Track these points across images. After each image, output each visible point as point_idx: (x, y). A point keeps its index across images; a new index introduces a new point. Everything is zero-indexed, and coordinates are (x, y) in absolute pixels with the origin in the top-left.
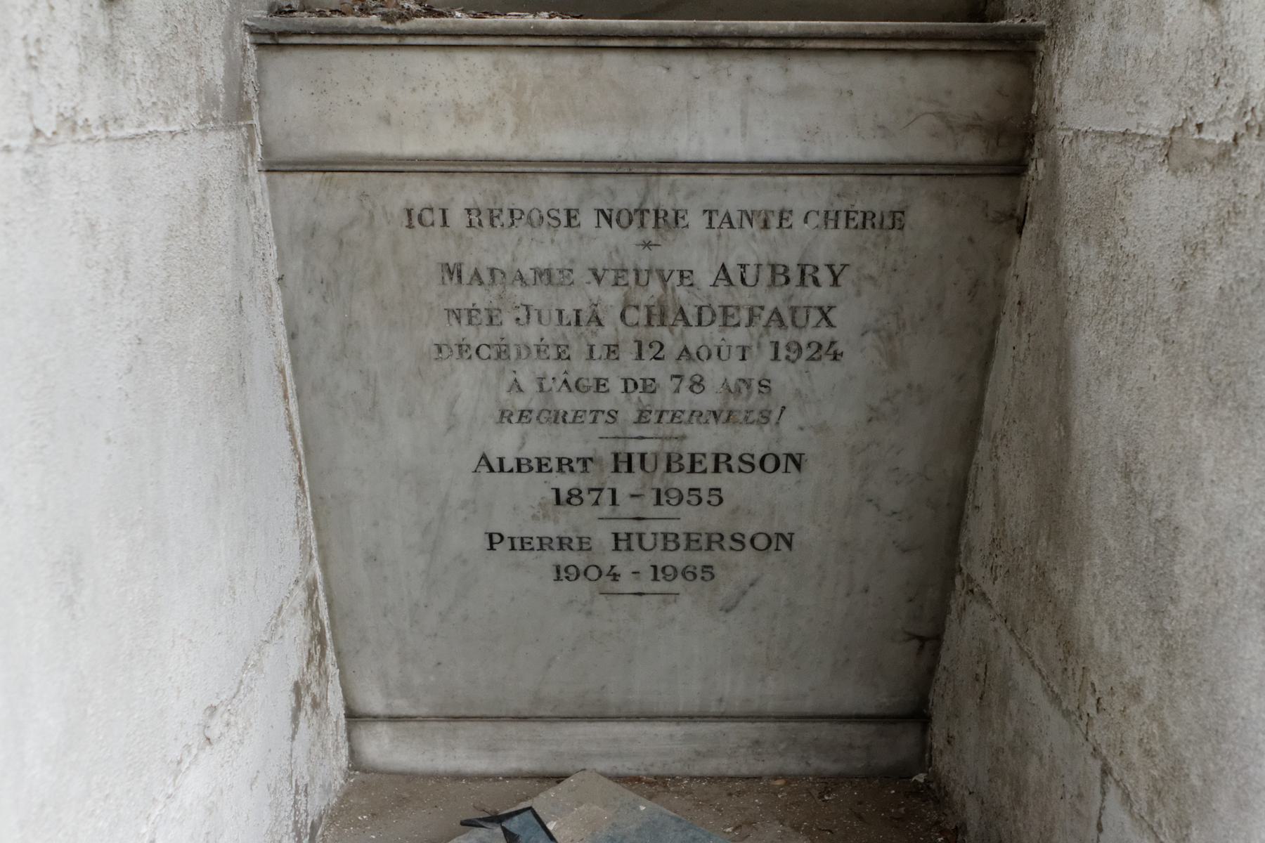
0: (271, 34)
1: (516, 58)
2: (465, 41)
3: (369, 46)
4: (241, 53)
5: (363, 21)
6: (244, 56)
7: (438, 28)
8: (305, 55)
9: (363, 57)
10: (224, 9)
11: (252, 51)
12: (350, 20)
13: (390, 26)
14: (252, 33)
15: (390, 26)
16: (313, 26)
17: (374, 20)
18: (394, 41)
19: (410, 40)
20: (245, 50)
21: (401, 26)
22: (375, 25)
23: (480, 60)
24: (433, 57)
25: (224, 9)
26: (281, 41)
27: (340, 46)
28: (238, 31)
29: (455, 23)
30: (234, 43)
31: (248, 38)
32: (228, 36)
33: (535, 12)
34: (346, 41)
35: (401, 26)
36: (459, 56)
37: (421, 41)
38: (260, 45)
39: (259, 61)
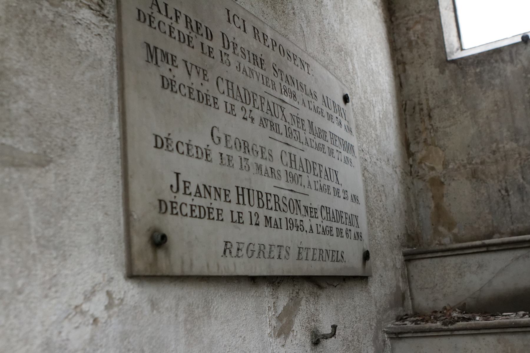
0: (395, 334)
1: (508, 337)
2: (481, 332)
3: (431, 336)
4: (382, 344)
5: (433, 325)
6: (384, 345)
7: (468, 326)
8: (410, 341)
9: (436, 341)
10: (373, 328)
11: (388, 342)
12: (429, 325)
13: (446, 327)
14: (387, 334)
15: (446, 327)
16: (412, 329)
17: (439, 324)
18: (449, 333)
19: (456, 333)
20: (384, 341)
21: (450, 327)
22: (439, 327)
23: (491, 340)
24: (468, 339)
25: (373, 328)
26: (400, 336)
27: (505, 332)
28: (380, 334)
29: (475, 324)
30: (379, 340)
31: (386, 336)
32: (376, 338)
33: (516, 311)
34: (427, 334)
35: (450, 327)
36: (480, 338)
37: (461, 332)
38: (391, 338)
39: (392, 345)
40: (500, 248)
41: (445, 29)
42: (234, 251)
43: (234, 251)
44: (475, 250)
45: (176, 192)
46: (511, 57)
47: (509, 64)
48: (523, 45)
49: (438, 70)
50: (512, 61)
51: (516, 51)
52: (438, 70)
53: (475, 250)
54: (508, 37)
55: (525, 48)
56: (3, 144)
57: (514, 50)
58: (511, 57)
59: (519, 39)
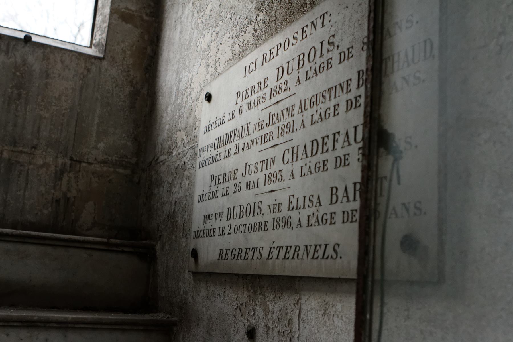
40: (15, 240)
41: (79, 51)
42: (285, 112)
43: (285, 112)
44: (36, 241)
45: (412, 23)
46: (8, 48)
47: (3, 54)
48: (23, 43)
49: (33, 68)
50: (7, 53)
51: (14, 46)
52: (33, 68)
53: (36, 241)
54: (10, 27)
55: (23, 47)
56: (313, 5)
57: (13, 43)
58: (8, 48)
59: (22, 36)
